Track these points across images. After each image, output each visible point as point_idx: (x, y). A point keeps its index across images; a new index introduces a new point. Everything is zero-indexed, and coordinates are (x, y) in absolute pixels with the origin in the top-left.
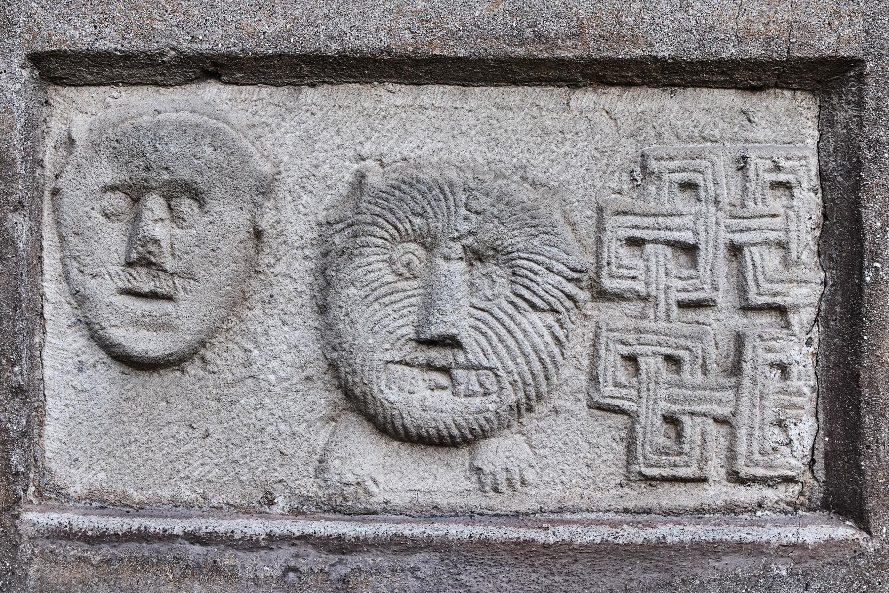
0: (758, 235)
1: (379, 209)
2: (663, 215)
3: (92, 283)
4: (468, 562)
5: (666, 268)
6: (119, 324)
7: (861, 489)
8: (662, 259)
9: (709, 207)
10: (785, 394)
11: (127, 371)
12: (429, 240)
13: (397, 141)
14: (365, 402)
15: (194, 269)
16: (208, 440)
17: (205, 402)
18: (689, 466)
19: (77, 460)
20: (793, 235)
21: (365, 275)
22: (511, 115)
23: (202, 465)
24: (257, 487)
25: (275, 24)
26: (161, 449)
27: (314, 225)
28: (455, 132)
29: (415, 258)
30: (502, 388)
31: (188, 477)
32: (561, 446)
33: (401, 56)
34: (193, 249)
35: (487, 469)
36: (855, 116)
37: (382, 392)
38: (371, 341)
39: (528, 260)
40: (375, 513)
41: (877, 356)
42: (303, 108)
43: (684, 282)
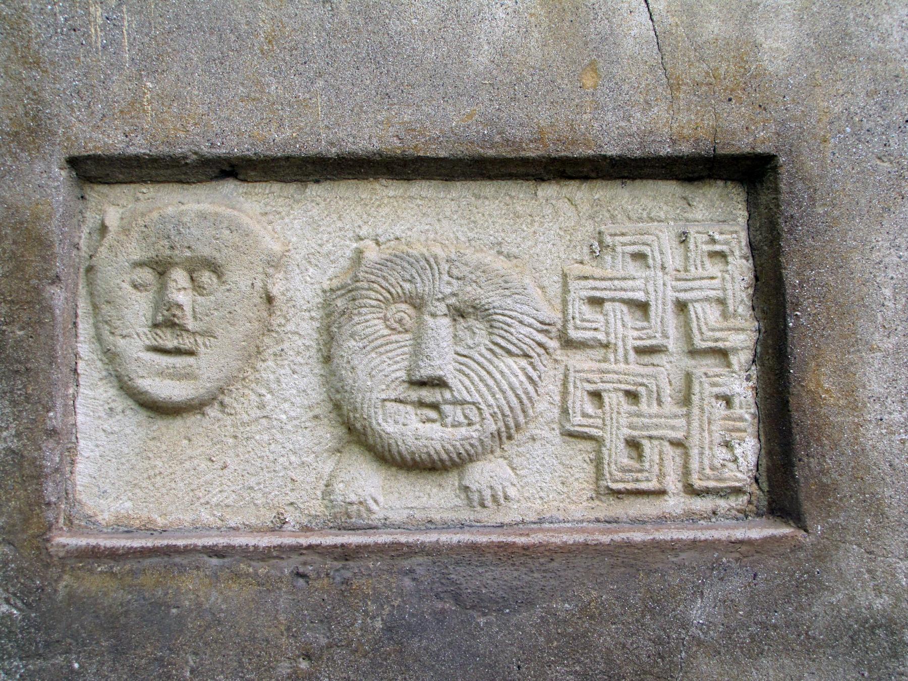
0: (699, 293)
1: (374, 277)
2: (618, 279)
3: (121, 342)
4: (458, 563)
5: (623, 321)
6: (146, 375)
7: (796, 494)
8: (619, 314)
9: (657, 272)
10: (729, 420)
11: (153, 416)
12: (418, 300)
13: (390, 225)
14: (365, 434)
15: (213, 328)
16: (226, 471)
17: (224, 439)
18: (650, 481)
19: (105, 492)
20: (730, 293)
21: (363, 330)
22: (487, 203)
23: (220, 492)
24: (270, 509)
25: (282, 133)
26: (183, 480)
27: (319, 292)
28: (440, 217)
29: (406, 316)
30: (484, 419)
31: (208, 503)
32: (538, 467)
33: (391, 157)
34: (212, 312)
35: (474, 487)
36: (774, 199)
37: (379, 425)
38: (369, 383)
39: (503, 315)
40: (376, 528)
41: (803, 386)
42: (309, 199)
43: (639, 332)
